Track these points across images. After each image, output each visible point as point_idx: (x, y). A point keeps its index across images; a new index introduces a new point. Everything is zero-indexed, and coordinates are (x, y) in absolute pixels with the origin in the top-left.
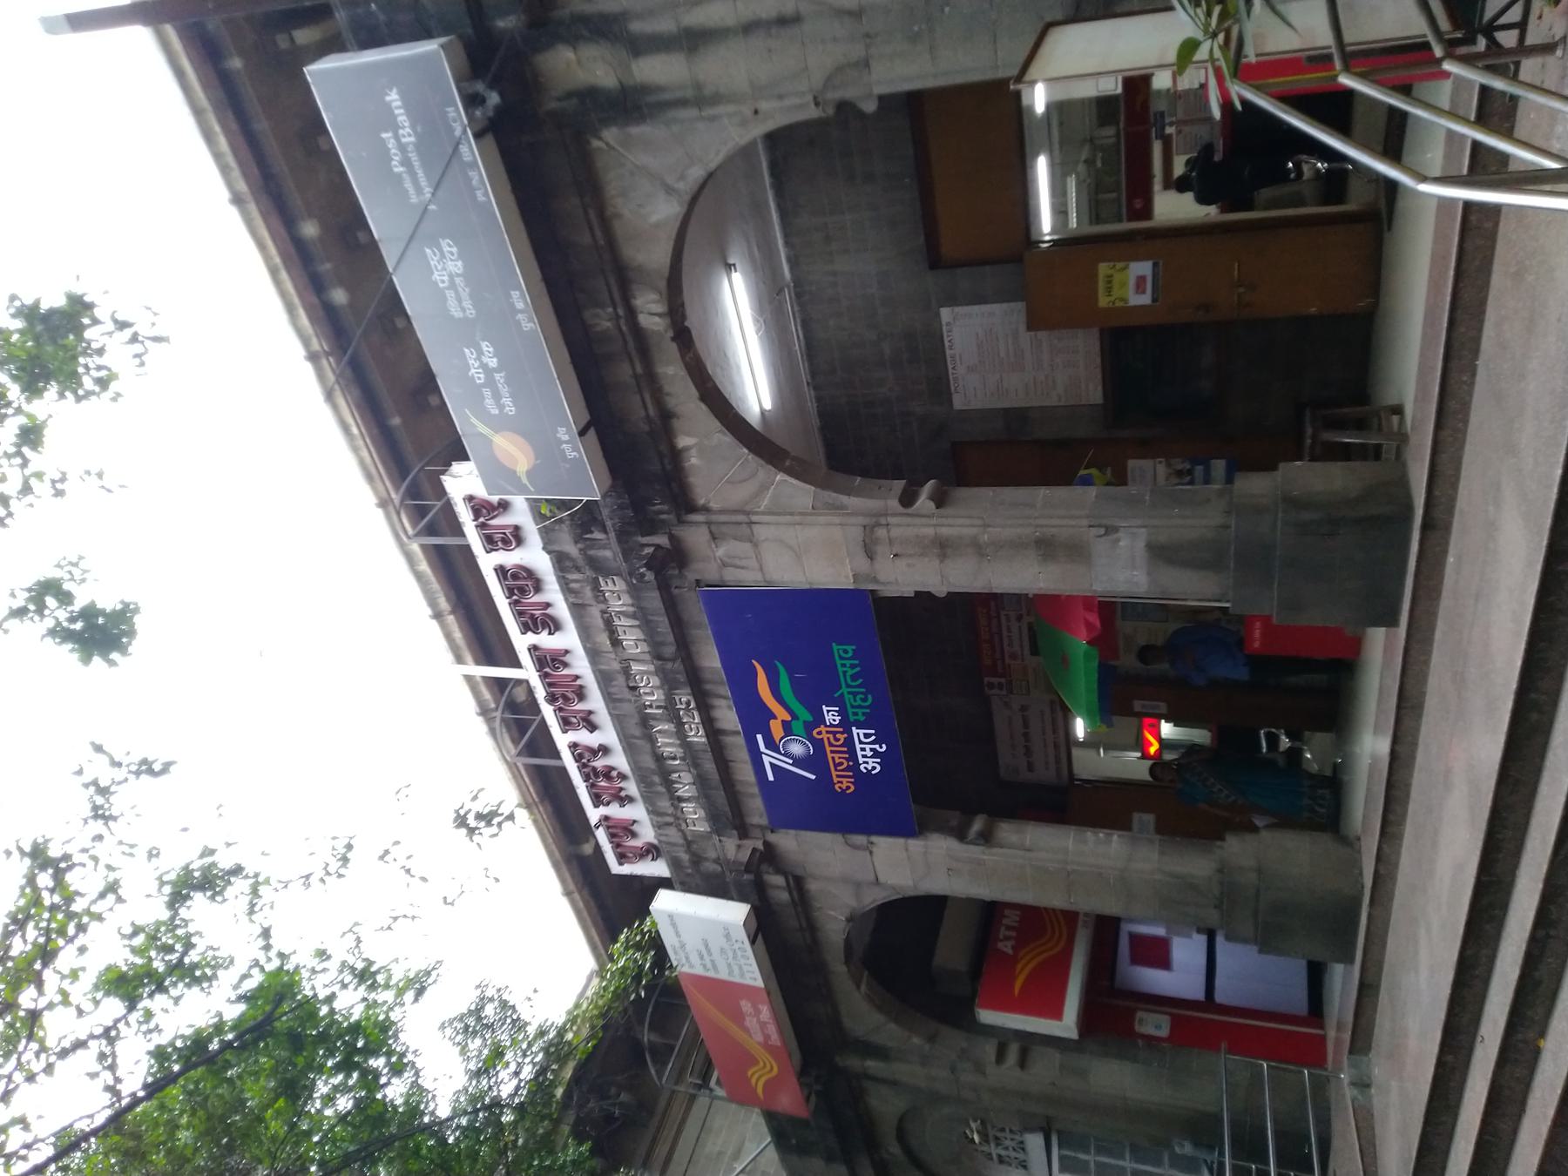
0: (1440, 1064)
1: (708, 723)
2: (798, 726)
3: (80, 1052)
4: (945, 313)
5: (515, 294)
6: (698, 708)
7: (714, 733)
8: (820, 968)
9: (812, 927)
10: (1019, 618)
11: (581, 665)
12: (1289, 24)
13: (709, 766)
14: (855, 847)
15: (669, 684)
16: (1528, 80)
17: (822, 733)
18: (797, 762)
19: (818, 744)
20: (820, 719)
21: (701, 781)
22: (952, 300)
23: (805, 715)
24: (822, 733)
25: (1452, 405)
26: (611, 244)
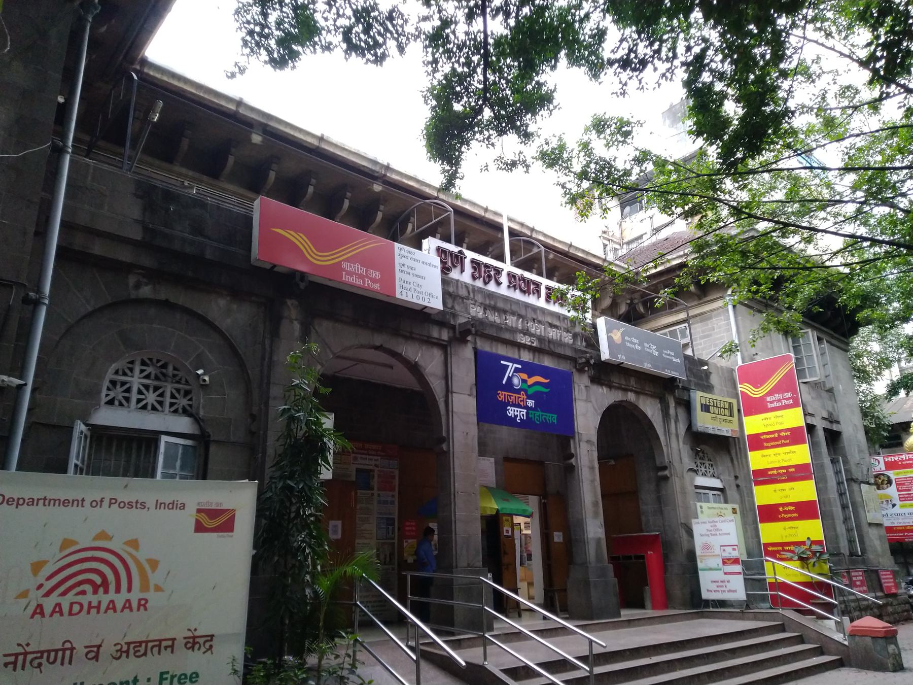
0: (625, 651)
1: (524, 346)
2: (525, 386)
3: (835, 250)
4: (492, 460)
5: (650, 366)
6: (531, 346)
7: (520, 346)
8: (396, 333)
9: (410, 337)
10: (376, 466)
11: (531, 300)
12: (711, 569)
13: (507, 336)
14: (471, 389)
15: (540, 339)
16: (488, 651)
17: (523, 396)
18: (510, 379)
19: (518, 392)
20: (530, 397)
21: (493, 325)
22: (496, 463)
23: (531, 391)
24: (523, 396)
25: (643, 621)
26: (646, 394)
